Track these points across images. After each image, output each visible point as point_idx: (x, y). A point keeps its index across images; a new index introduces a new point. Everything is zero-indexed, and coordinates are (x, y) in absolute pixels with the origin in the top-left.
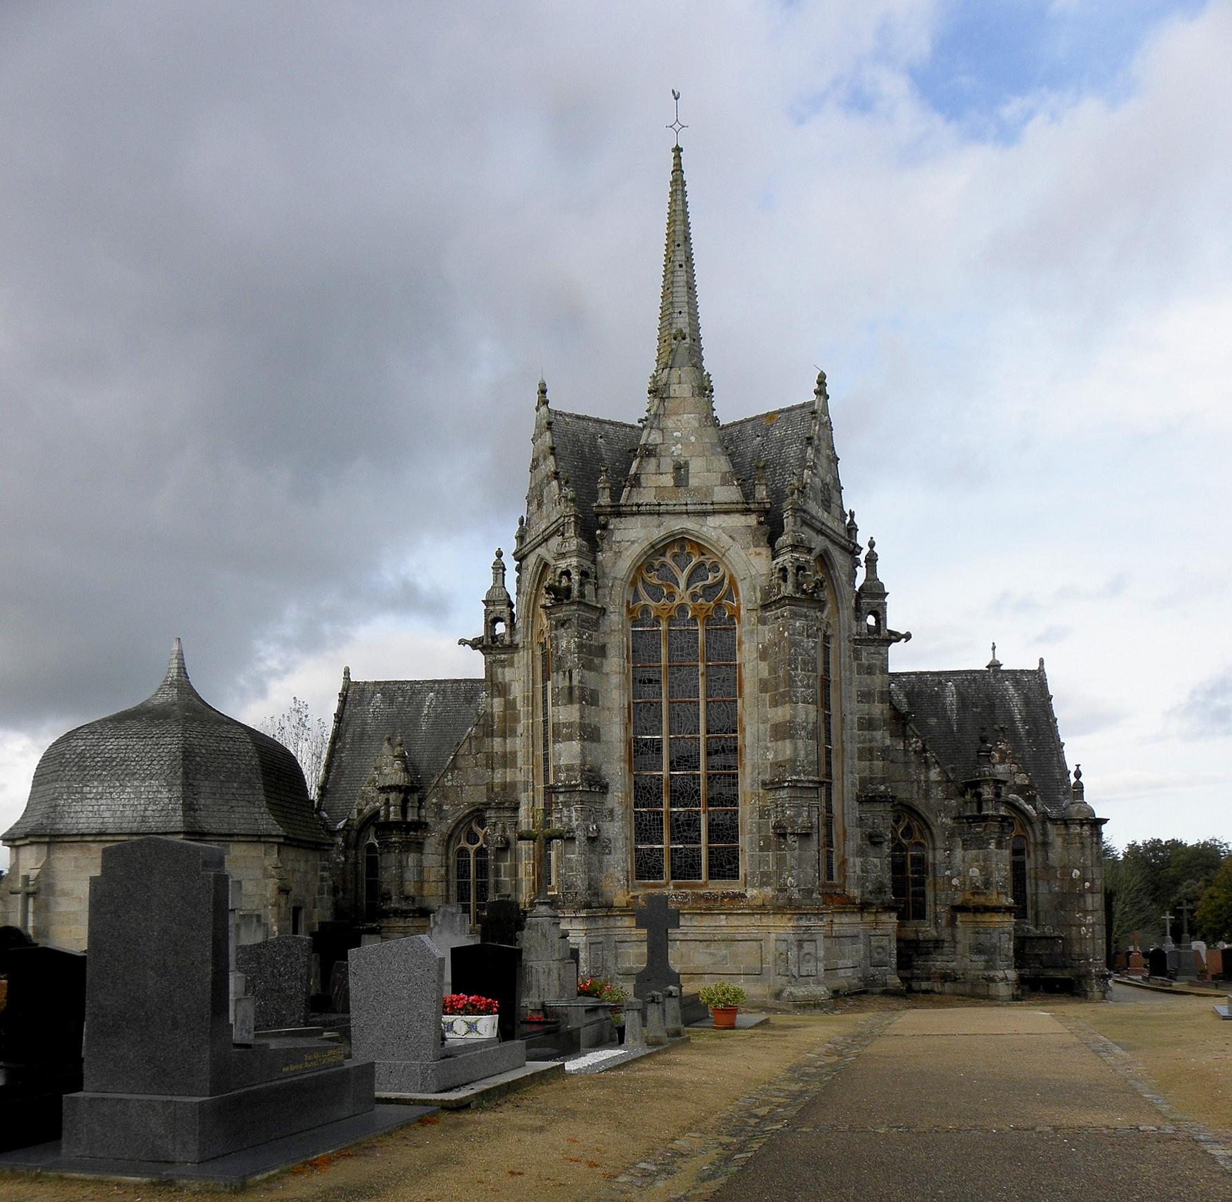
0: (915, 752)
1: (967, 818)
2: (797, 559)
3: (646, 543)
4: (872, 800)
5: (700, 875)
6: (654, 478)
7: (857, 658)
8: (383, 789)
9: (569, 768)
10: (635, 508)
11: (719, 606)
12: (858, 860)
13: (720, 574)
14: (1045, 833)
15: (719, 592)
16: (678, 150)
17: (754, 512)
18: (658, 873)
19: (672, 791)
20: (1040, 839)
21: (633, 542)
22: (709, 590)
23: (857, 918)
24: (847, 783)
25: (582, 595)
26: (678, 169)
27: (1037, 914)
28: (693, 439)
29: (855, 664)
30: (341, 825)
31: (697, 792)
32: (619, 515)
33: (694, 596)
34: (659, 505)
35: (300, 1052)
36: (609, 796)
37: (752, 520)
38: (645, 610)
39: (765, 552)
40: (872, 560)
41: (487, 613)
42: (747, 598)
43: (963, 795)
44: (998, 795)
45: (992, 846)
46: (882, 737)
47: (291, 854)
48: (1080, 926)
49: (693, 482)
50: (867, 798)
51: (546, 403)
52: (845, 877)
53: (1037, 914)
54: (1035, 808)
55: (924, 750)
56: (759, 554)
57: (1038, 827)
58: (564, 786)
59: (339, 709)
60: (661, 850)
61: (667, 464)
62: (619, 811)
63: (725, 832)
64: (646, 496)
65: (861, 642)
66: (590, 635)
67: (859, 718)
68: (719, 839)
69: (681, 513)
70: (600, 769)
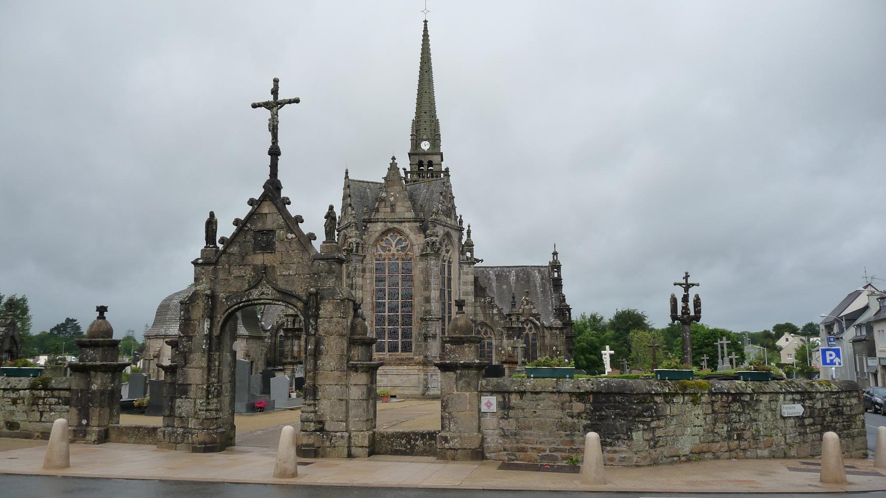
8: (286, 315)
11: (406, 254)
14: (543, 332)
16: (426, 22)
18: (384, 350)
19: (389, 320)
22: (403, 249)
25: (357, 251)
26: (426, 30)
30: (269, 328)
32: (371, 222)
33: (398, 251)
35: (261, 398)
37: (418, 224)
38: (380, 255)
39: (422, 235)
40: (469, 232)
42: (417, 251)
44: (518, 319)
47: (251, 341)
59: (271, 162)
61: (388, 204)
63: (406, 335)
64: (380, 216)
68: (405, 338)
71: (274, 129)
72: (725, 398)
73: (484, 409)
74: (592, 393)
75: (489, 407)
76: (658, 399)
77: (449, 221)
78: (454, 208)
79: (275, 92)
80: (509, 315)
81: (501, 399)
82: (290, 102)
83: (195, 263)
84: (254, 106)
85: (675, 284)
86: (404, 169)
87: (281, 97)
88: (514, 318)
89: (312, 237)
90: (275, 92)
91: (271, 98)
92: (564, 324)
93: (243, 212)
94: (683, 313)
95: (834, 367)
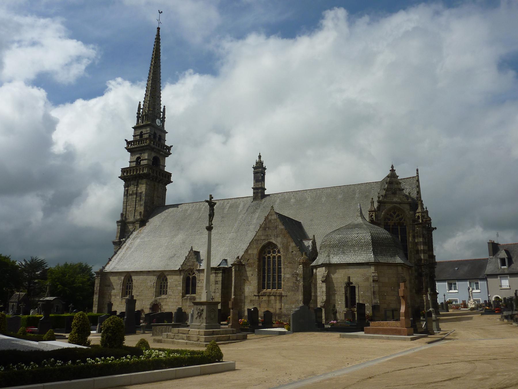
26: (158, 35)
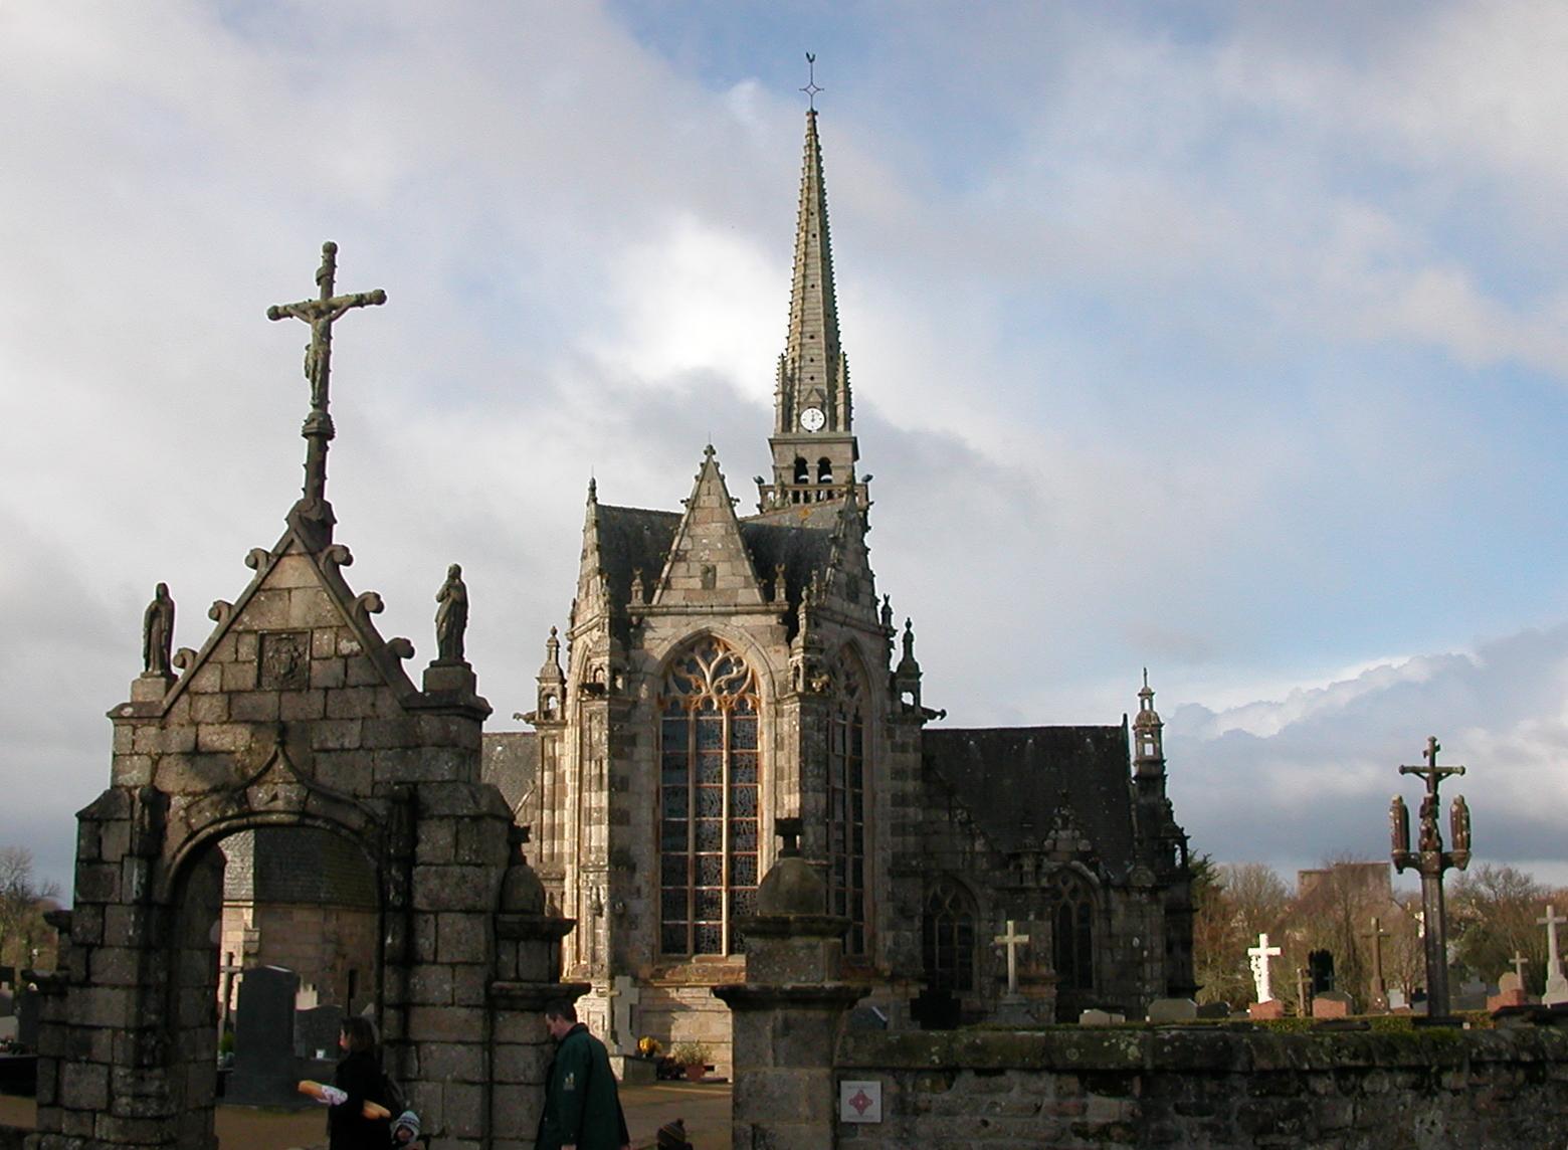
0: (960, 823)
1: (1010, 890)
2: (809, 659)
3: (675, 641)
4: (903, 875)
5: (721, 949)
6: (683, 580)
7: (891, 736)
9: (600, 849)
10: (665, 610)
12: (890, 935)
13: (743, 668)
14: (1107, 901)
15: (741, 685)
17: (773, 613)
20: (1103, 906)
21: (664, 640)
22: (732, 685)
23: (888, 990)
24: (878, 859)
27: (1100, 984)
28: (719, 545)
29: (888, 743)
31: (720, 871)
33: (719, 690)
34: (687, 606)
36: (638, 875)
39: (783, 649)
40: (908, 639)
41: (541, 690)
43: (1007, 866)
44: (1039, 867)
45: (1032, 917)
46: (915, 814)
48: (1139, 995)
49: (719, 584)
50: (898, 869)
51: (595, 500)
52: (875, 950)
53: (1100, 984)
54: (1097, 875)
55: (969, 822)
56: (778, 651)
57: (1101, 893)
58: (593, 866)
60: (685, 926)
61: (697, 569)
62: (645, 890)
65: (895, 722)
66: (621, 727)
67: (893, 796)
69: (707, 614)
70: (629, 849)
71: (319, 372)
72: (1506, 1076)
73: (848, 1113)
74: (1140, 1071)
75: (861, 1109)
76: (1321, 1085)
77: (852, 610)
78: (869, 576)
79: (326, 278)
80: (1016, 856)
81: (893, 1089)
82: (360, 301)
83: (116, 715)
84: (276, 314)
85: (1404, 770)
86: (760, 481)
87: (338, 292)
88: (1028, 864)
89: (405, 649)
90: (326, 278)
91: (315, 294)
92: (1159, 877)
93: (236, 583)
94: (1424, 848)
95: (330, 948)
